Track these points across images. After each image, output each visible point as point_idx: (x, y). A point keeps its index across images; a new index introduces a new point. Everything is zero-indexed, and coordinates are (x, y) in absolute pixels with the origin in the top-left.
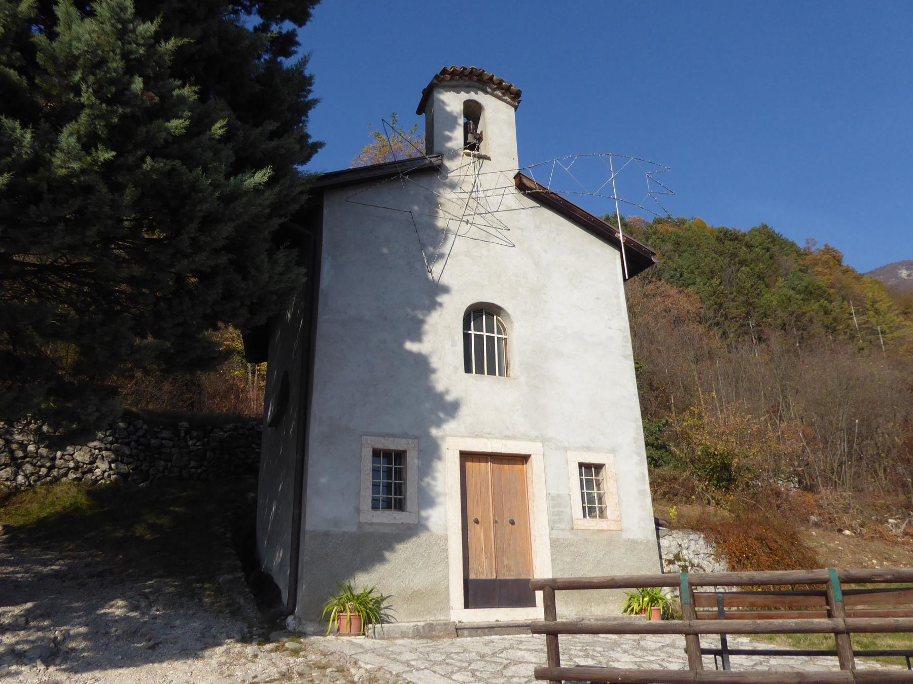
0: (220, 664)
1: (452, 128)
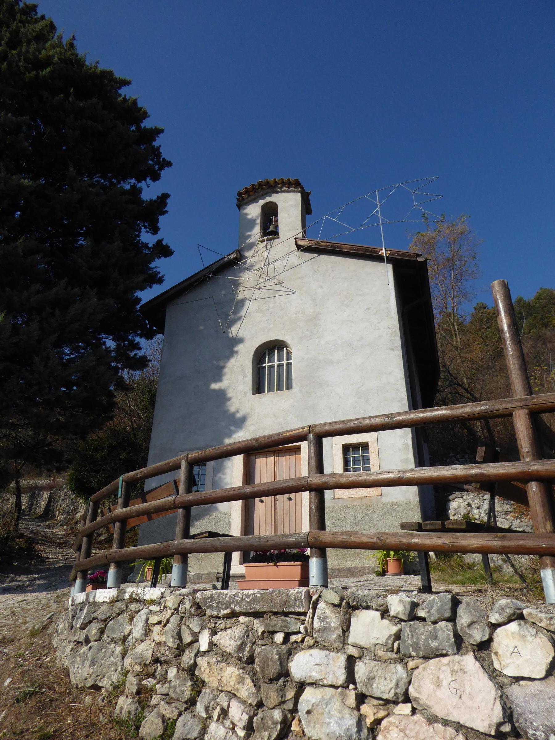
1: (251, 228)
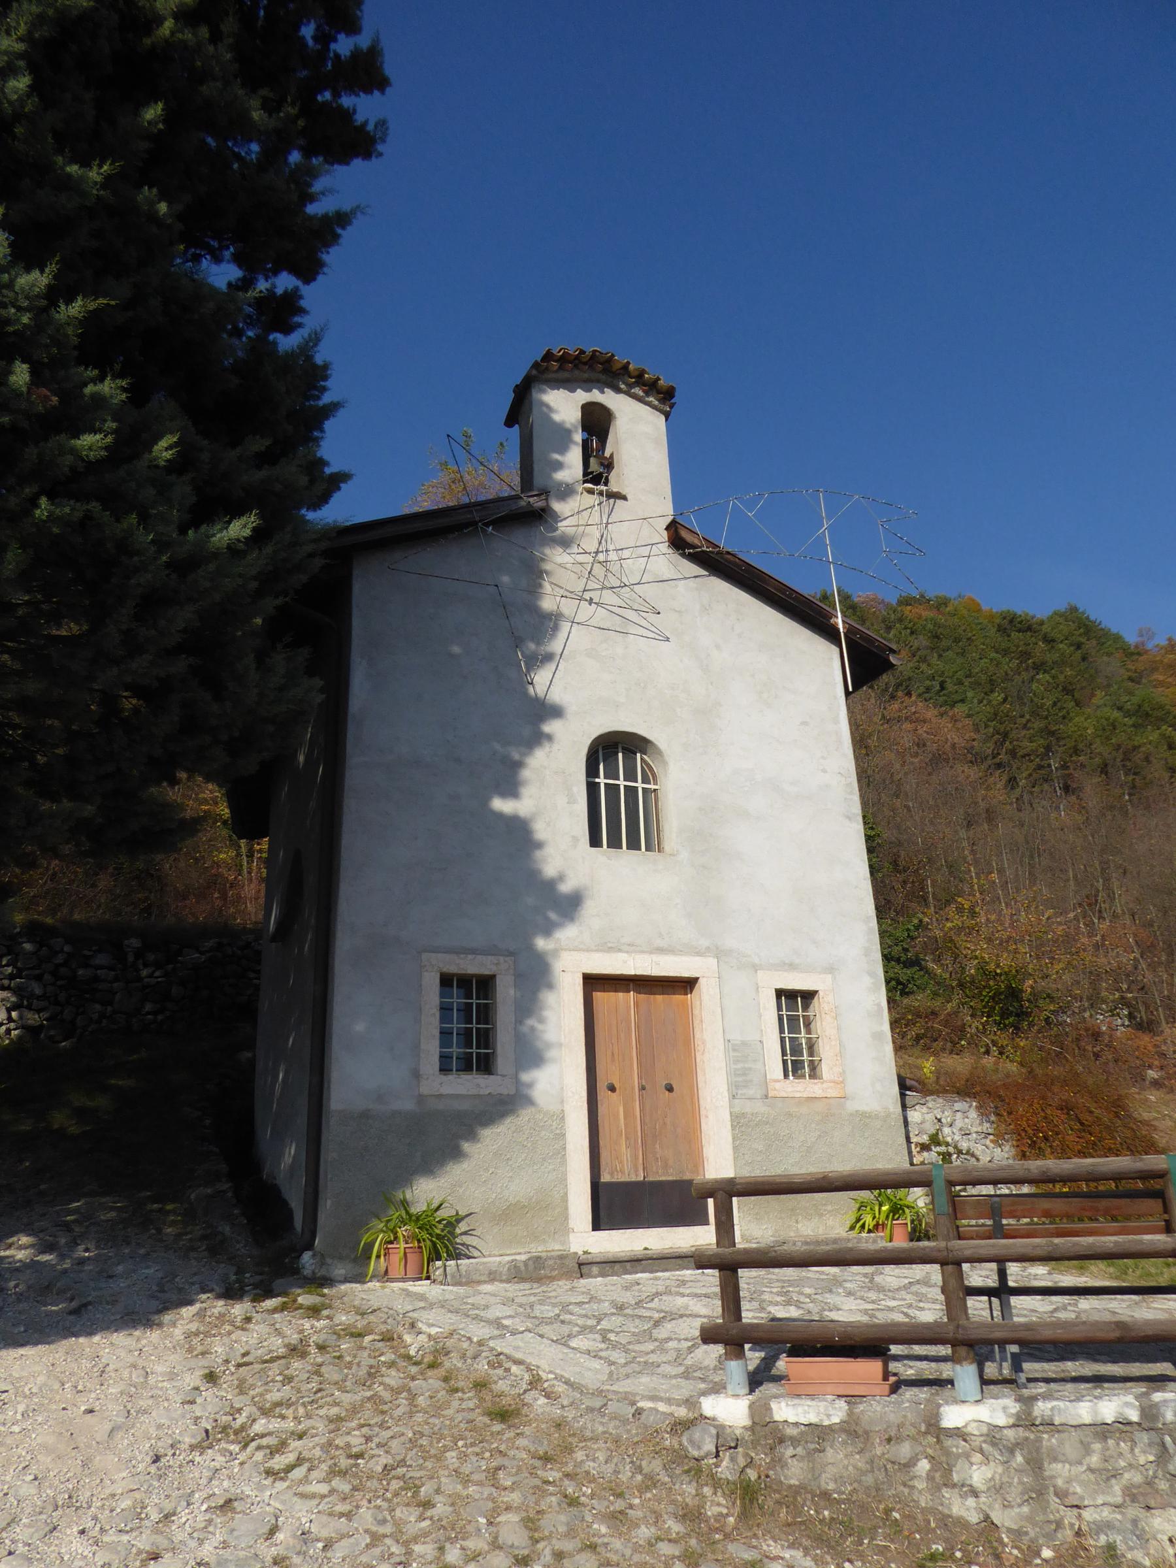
0: (188, 1335)
1: (563, 448)
